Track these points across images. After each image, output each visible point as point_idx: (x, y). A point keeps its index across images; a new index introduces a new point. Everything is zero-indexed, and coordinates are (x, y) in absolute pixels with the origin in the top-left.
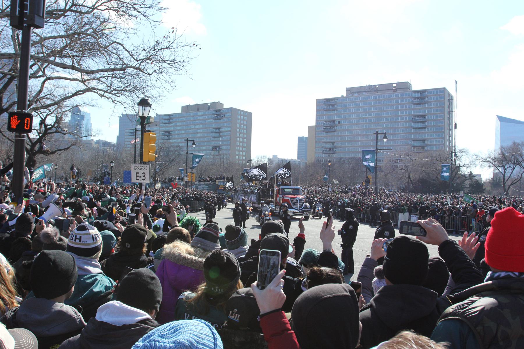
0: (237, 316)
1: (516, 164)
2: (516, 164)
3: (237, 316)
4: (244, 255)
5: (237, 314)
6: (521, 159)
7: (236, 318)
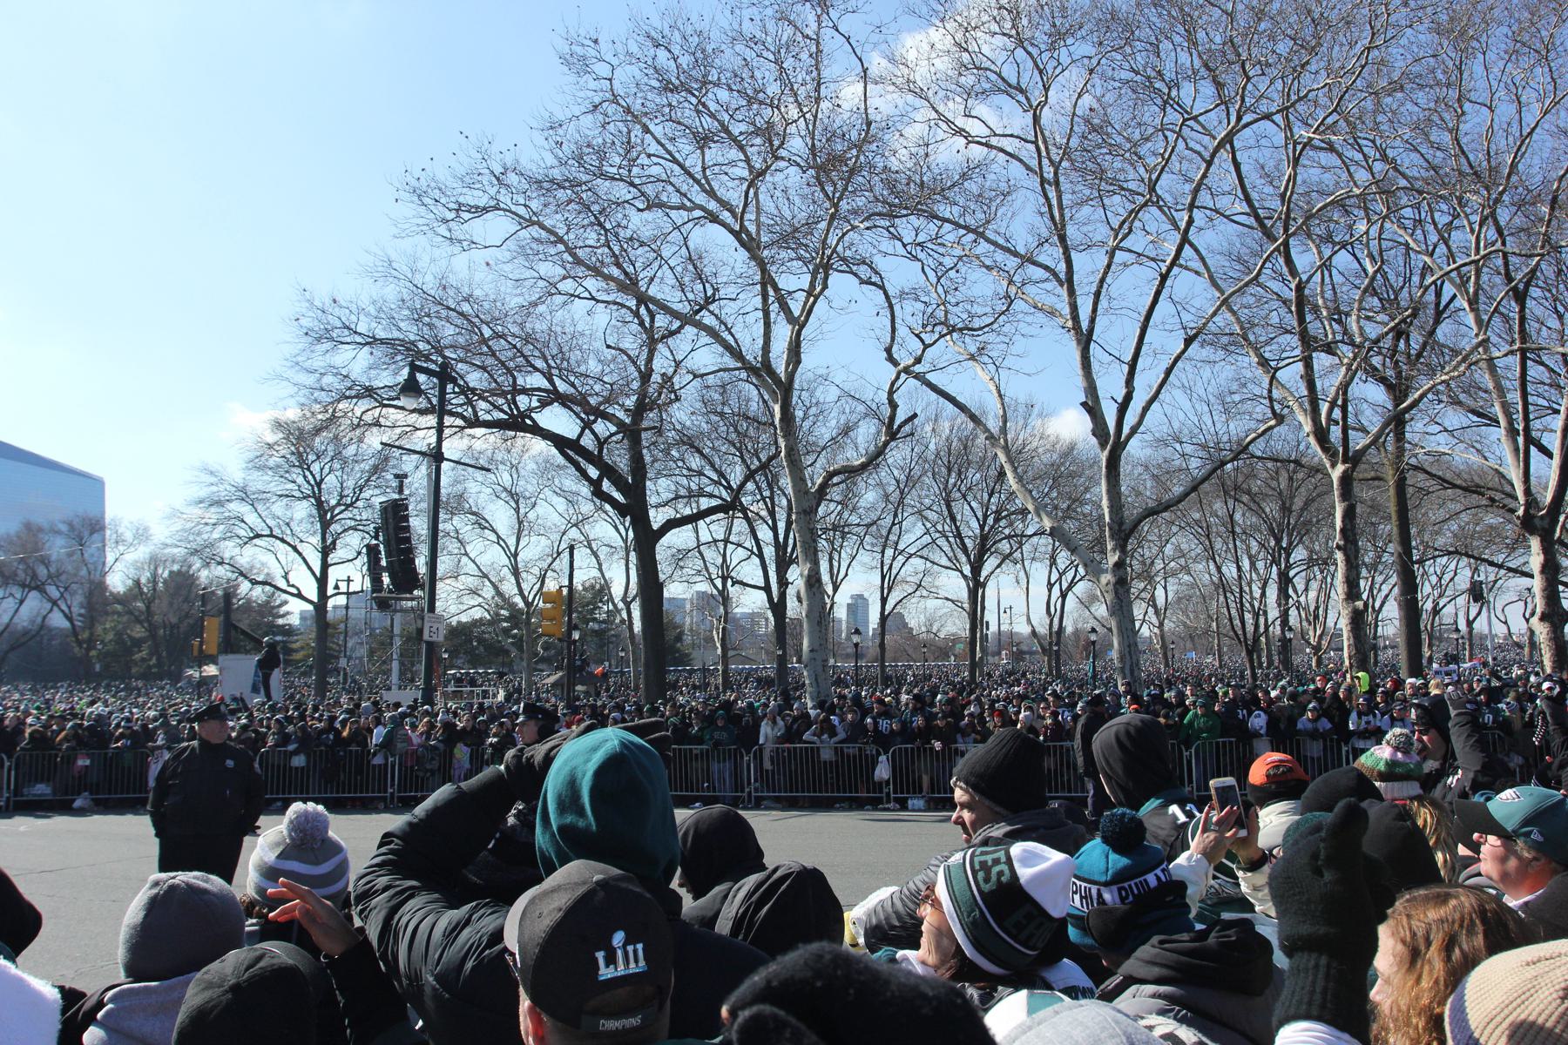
0: (635, 951)
1: (29, 586)
2: (29, 586)
3: (635, 951)
4: (259, 771)
5: (630, 948)
6: (45, 571)
7: (632, 965)
